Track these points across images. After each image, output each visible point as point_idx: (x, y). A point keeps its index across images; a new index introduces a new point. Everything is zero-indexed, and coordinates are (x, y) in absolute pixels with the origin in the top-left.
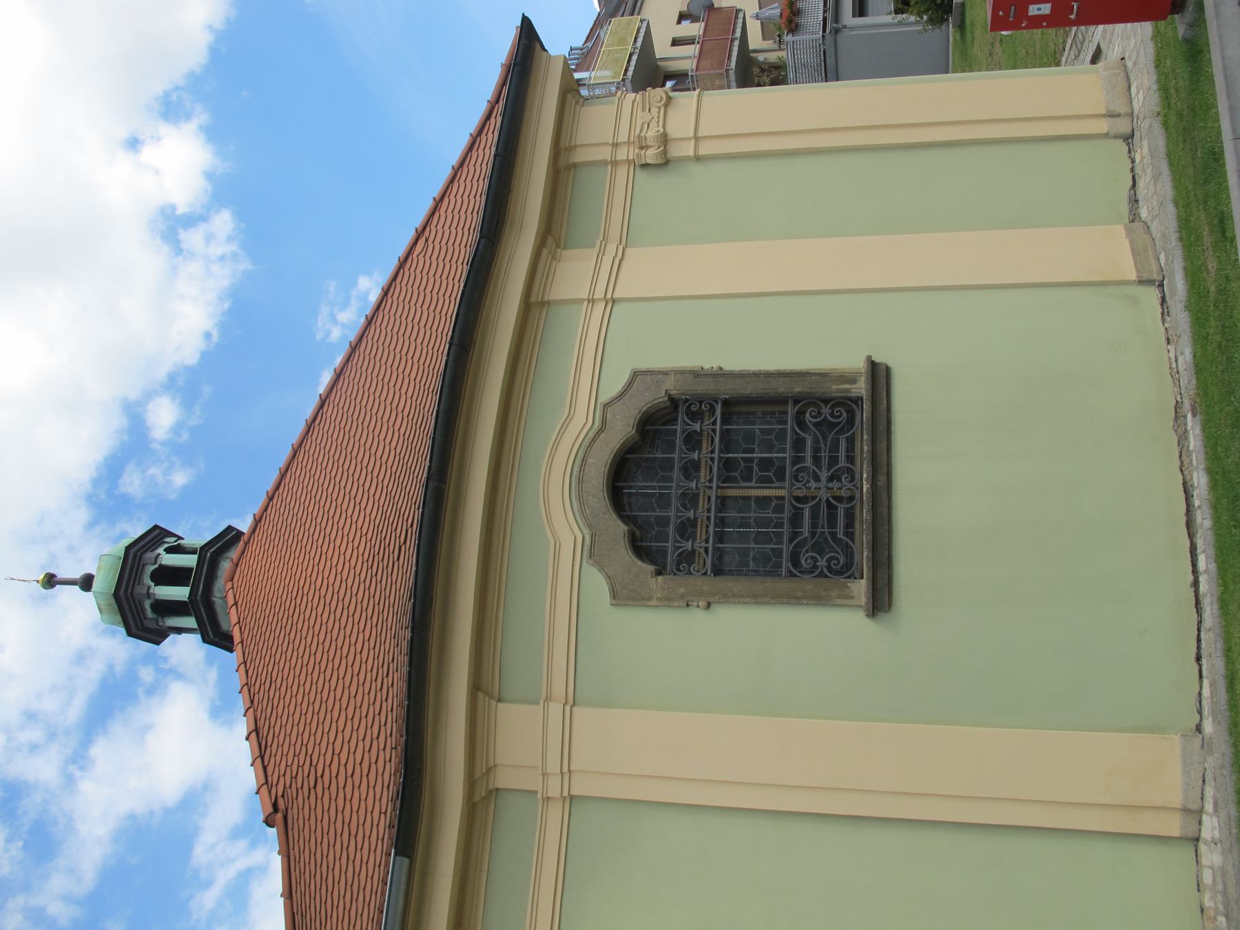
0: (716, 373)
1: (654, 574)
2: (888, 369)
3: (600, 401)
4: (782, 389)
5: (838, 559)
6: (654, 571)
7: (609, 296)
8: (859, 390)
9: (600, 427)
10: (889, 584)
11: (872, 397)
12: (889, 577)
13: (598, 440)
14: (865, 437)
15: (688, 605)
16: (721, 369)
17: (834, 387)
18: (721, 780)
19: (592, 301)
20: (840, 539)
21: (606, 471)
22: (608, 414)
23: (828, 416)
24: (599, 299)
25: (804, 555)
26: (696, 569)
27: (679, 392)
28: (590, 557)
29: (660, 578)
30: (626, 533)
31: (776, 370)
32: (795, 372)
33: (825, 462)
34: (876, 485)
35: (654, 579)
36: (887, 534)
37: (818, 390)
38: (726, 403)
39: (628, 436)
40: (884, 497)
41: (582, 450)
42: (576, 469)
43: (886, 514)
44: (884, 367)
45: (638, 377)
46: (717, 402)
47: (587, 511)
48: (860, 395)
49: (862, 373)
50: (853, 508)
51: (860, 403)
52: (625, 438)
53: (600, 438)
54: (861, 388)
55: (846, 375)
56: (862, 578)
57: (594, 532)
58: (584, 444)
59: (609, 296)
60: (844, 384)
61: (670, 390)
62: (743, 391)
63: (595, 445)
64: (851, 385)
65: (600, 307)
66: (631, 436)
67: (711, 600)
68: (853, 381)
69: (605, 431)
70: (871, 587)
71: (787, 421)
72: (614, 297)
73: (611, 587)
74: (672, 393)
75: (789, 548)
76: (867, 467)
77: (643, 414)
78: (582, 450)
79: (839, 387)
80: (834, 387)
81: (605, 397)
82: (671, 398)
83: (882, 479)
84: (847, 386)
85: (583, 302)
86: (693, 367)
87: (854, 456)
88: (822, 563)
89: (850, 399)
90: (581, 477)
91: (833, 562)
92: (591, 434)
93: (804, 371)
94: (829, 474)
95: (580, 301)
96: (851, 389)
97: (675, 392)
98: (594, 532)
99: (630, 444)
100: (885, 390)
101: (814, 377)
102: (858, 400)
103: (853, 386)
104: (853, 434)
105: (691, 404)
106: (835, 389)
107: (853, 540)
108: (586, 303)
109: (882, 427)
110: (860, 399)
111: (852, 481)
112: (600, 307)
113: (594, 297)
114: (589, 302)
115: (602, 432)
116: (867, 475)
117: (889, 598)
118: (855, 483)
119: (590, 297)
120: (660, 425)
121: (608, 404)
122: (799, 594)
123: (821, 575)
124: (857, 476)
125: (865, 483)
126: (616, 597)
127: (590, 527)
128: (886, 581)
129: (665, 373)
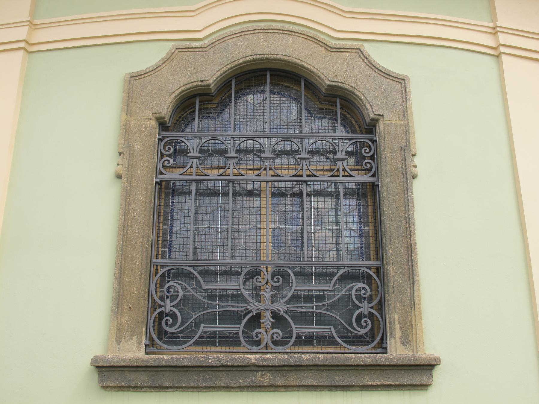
0: (408, 171)
1: (157, 115)
2: (424, 387)
3: (366, 46)
4: (390, 251)
5: (172, 326)
6: (161, 115)
7: (503, 49)
8: (393, 350)
9: (332, 46)
10: (129, 387)
11: (379, 365)
12: (168, 388)
13: (316, 45)
14: (321, 356)
15: (120, 154)
16: (414, 177)
17: (396, 317)
18: (150, 257)
19: (495, 31)
20: (200, 327)
21: (279, 57)
22: (348, 54)
23: (360, 310)
24: (497, 39)
25: (178, 283)
26: (166, 163)
27: (382, 132)
28: (177, 49)
29: (153, 123)
30: (205, 83)
31: (415, 243)
32: (415, 267)
33: (300, 307)
34: (257, 371)
35: (151, 117)
36: (192, 385)
37: (393, 296)
38: (374, 186)
39: (322, 76)
40: (242, 382)
41: (302, 29)
42: (280, 26)
43: (219, 383)
44: (425, 381)
45: (399, 84)
46: (373, 176)
47: (230, 41)
48: (388, 350)
49: (417, 352)
50: (239, 344)
51: (379, 350)
52: (319, 73)
53: (319, 47)
54: (396, 351)
55: (414, 332)
56: (147, 353)
57: (206, 50)
58: (311, 31)
59: (503, 49)
60: (401, 328)
61: (383, 121)
62: (386, 204)
63: (311, 43)
64: (400, 339)
65: (489, 41)
66: (322, 80)
67: (124, 179)
68: (406, 341)
69: (327, 52)
70: (123, 364)
71: (229, 194)
72: (503, 56)
73: (144, 72)
74: (381, 122)
75: (190, 266)
76: (279, 359)
77: (352, 92)
78: (302, 29)
79: (397, 322)
80: (396, 317)
81: (368, 48)
82: (374, 123)
83: (265, 378)
84: (398, 333)
85: (492, 22)
86: (414, 144)
87: (313, 345)
88: (168, 306)
89: (383, 339)
90: (271, 31)
91: (171, 320)
92: (322, 37)
93: (416, 278)
94: (282, 313)
95: (494, 17)
96: (395, 339)
97: (382, 126)
98: (206, 50)
99: (317, 83)
100: (391, 383)
101: (409, 290)
102: (382, 347)
103: (398, 339)
104: (336, 343)
105: (370, 147)
106: (394, 319)
107: (196, 344)
108: (491, 25)
109: (338, 378)
110: (385, 351)
111: (275, 343)
112: (489, 41)
113: (499, 34)
114: (494, 28)
115: (325, 48)
116: (268, 359)
117: (114, 387)
118: (272, 346)
119: (499, 29)
120: (341, 114)
121: (362, 52)
122: (126, 278)
123: (154, 305)
124: (280, 349)
125: (258, 356)
126: (133, 79)
127: (212, 45)
128: (133, 384)
129: (405, 113)
